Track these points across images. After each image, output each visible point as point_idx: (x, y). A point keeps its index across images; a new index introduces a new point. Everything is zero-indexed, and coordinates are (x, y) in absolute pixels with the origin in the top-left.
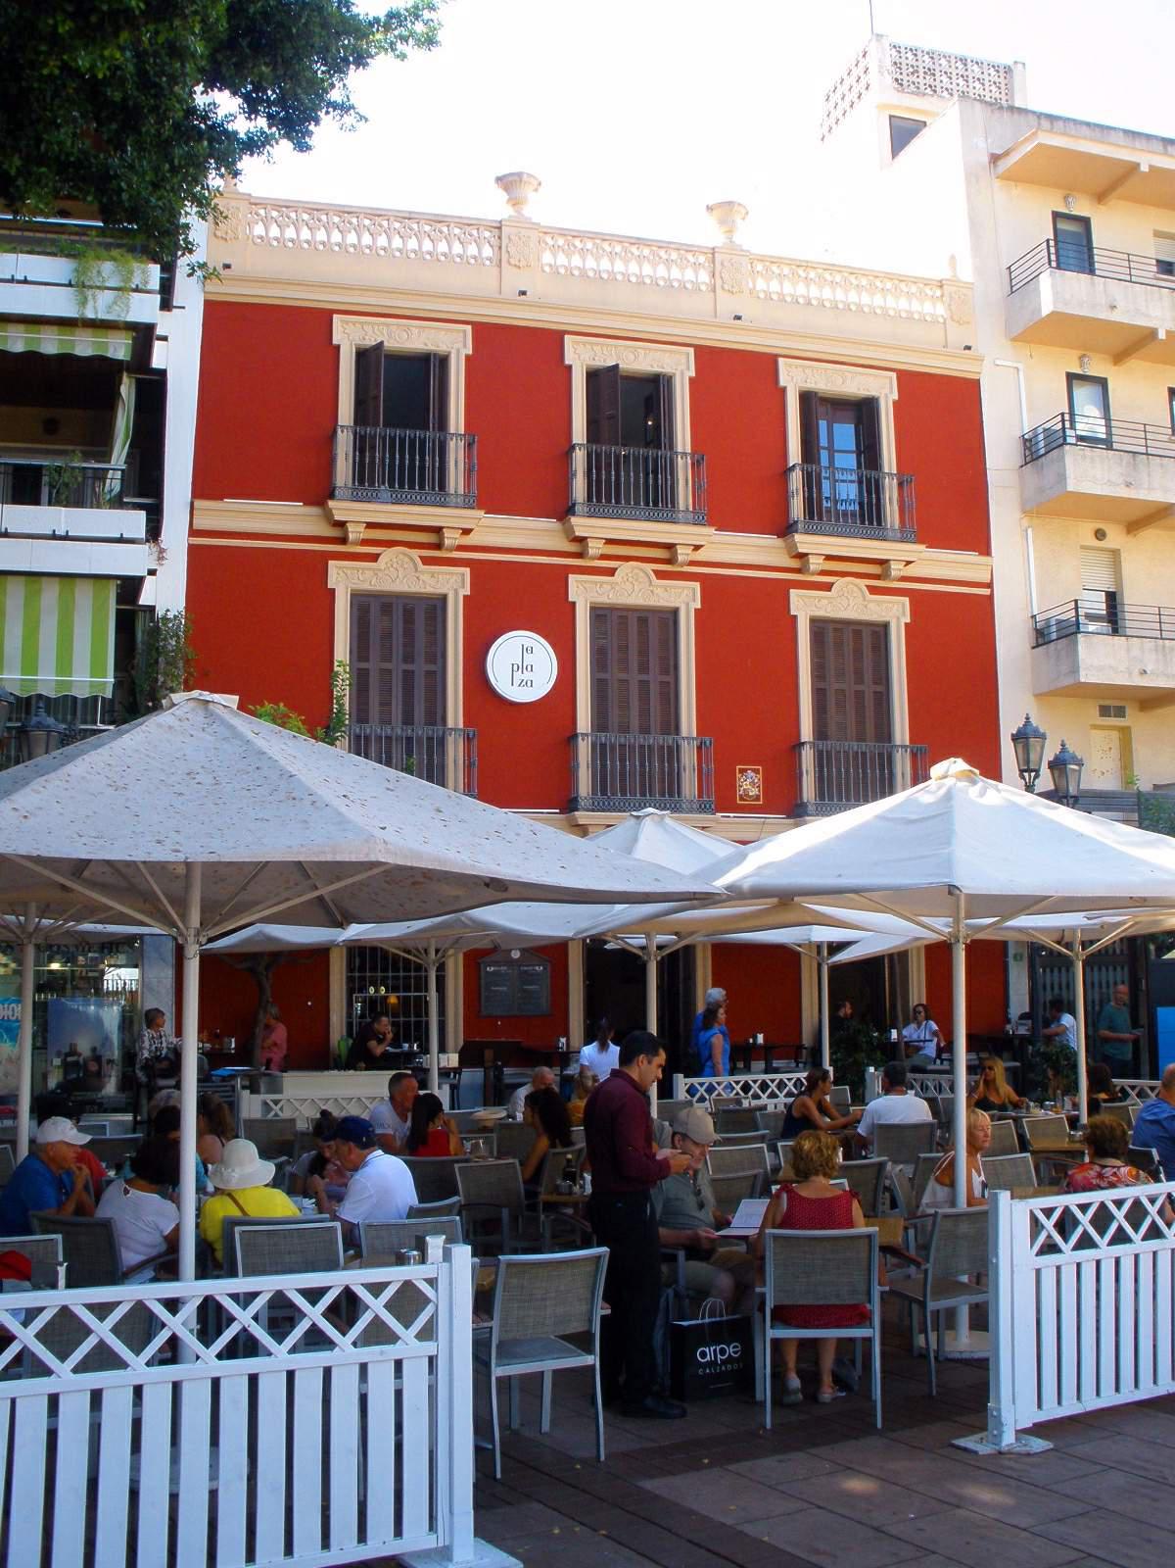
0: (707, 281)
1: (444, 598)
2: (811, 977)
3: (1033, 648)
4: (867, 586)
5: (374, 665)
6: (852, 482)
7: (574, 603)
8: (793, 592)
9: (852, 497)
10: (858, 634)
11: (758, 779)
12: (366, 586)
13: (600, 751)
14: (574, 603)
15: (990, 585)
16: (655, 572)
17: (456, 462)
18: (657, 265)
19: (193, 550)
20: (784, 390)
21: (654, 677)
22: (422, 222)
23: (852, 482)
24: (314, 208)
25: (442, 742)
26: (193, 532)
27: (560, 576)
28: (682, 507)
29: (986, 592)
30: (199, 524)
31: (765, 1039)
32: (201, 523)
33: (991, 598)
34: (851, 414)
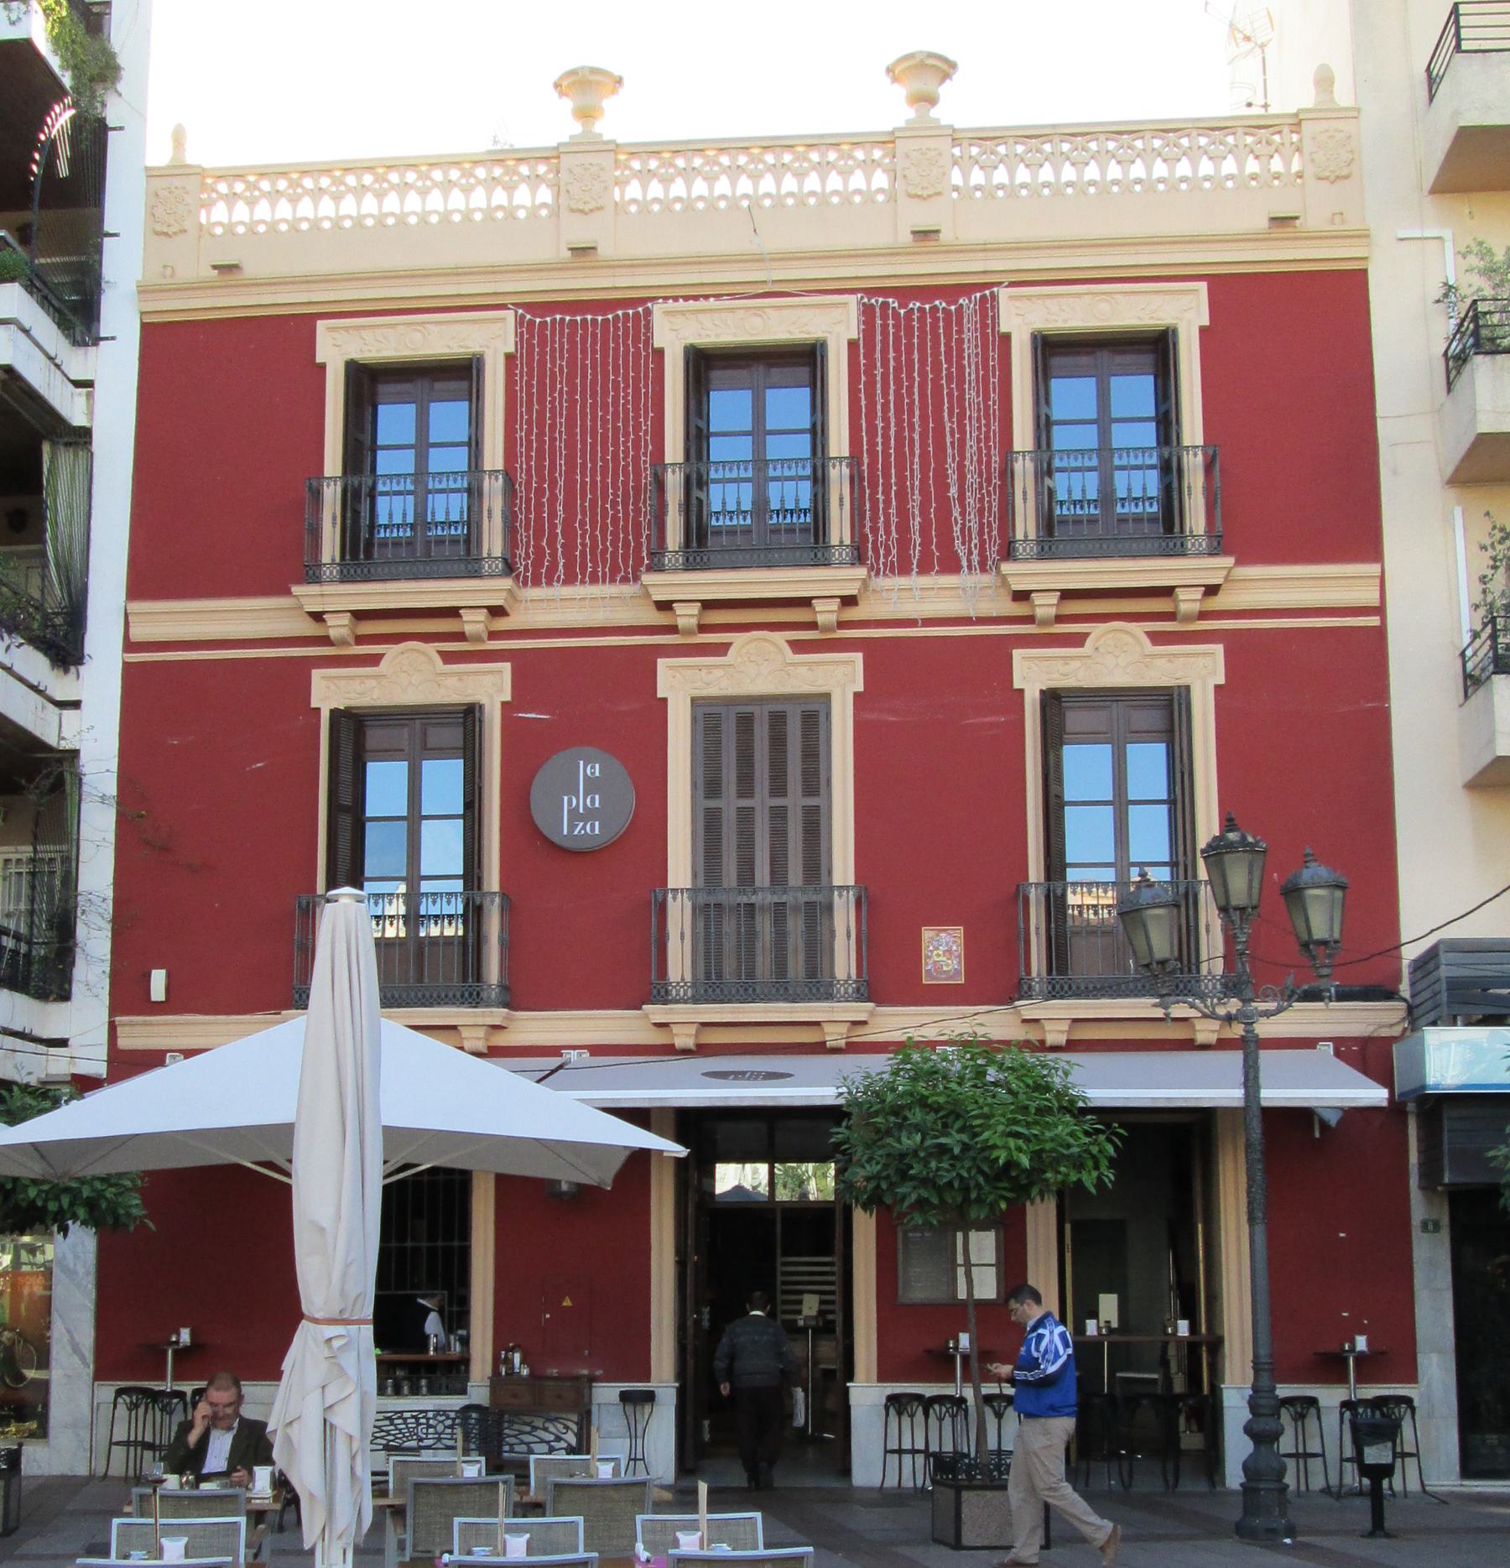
0: (885, 185)
1: (827, 697)
2: (1238, 1238)
3: (1461, 706)
4: (1148, 633)
5: (729, 803)
6: (1152, 467)
7: (665, 700)
8: (1017, 654)
9: (455, 517)
10: (745, 723)
11: (958, 948)
12: (713, 691)
13: (707, 913)
14: (665, 700)
15: (1380, 610)
16: (441, 653)
17: (1025, 493)
18: (716, 178)
19: (129, 670)
20: (322, 367)
21: (795, 800)
22: (1240, 131)
23: (1152, 467)
24: (1167, 129)
25: (829, 908)
26: (130, 646)
27: (641, 665)
28: (834, 541)
29: (1374, 621)
30: (137, 634)
31: (193, 1335)
32: (139, 633)
33: (1380, 633)
34: (1148, 359)
